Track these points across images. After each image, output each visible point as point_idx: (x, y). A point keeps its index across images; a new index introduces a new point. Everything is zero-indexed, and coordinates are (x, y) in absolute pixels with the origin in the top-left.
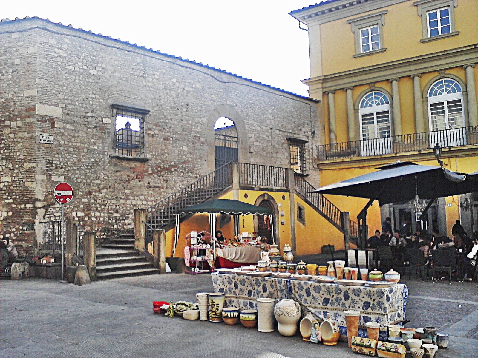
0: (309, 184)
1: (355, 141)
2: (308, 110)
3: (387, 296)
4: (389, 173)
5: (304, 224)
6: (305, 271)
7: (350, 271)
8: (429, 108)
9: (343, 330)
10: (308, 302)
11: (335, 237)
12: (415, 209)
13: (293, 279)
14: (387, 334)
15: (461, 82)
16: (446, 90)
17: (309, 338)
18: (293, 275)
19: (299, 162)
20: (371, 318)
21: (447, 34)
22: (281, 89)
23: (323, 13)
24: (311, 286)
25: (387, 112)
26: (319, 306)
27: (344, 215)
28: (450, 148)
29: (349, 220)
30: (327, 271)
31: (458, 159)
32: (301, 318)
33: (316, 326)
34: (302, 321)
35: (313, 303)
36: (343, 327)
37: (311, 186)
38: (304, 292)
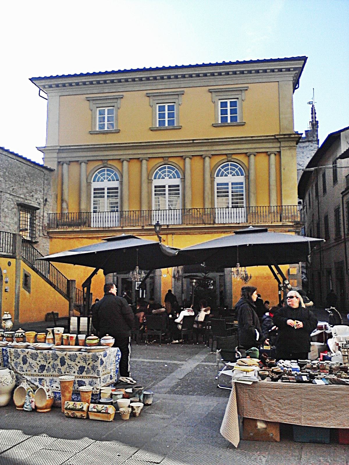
0: (38, 252)
1: (86, 213)
2: (42, 177)
3: (101, 359)
4: (120, 244)
5: (29, 292)
6: (23, 339)
7: (68, 337)
8: (153, 189)
9: (58, 395)
10: (24, 370)
11: (59, 303)
12: (135, 278)
13: (10, 348)
14: (99, 396)
15: (180, 170)
16: (231, 173)
17: (22, 406)
18: (10, 343)
19: (28, 228)
20: (85, 382)
21: (173, 127)
22: (16, 153)
23: (64, 85)
24: (28, 353)
25: (117, 188)
26: (35, 373)
27: (70, 283)
28: (168, 226)
29: (75, 288)
30: (45, 338)
31: (174, 236)
32: (16, 386)
33: (31, 393)
34: (16, 390)
35: (29, 371)
36: (58, 392)
37: (39, 253)
38: (20, 360)
